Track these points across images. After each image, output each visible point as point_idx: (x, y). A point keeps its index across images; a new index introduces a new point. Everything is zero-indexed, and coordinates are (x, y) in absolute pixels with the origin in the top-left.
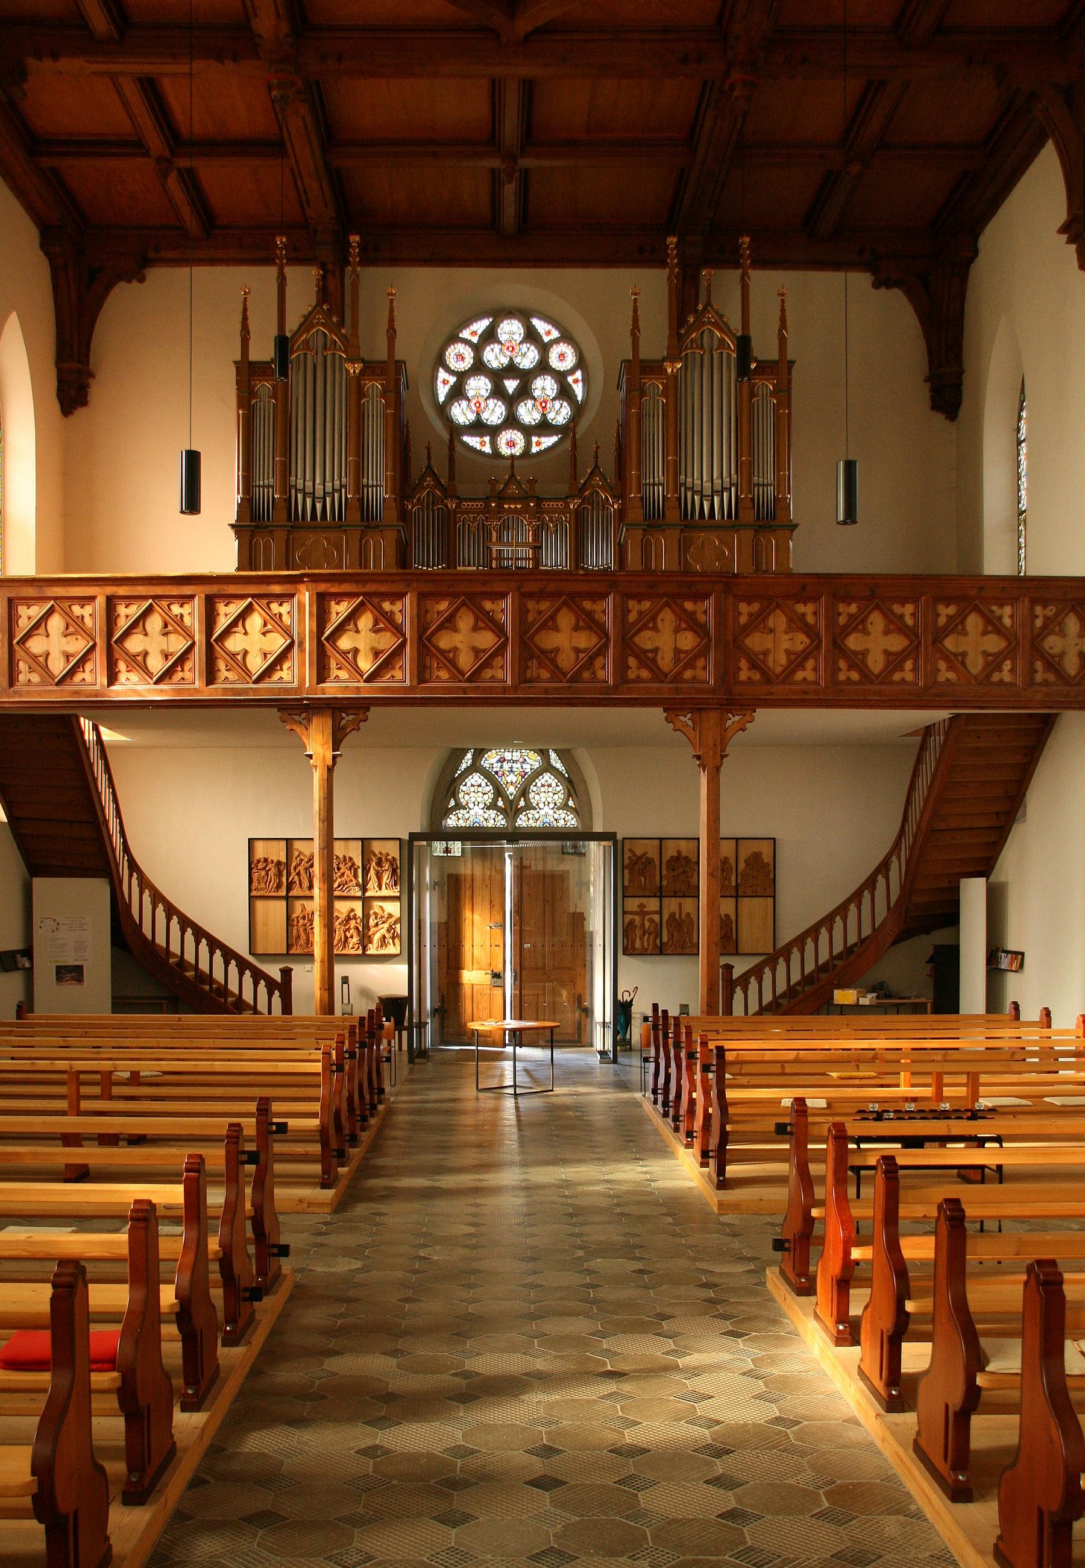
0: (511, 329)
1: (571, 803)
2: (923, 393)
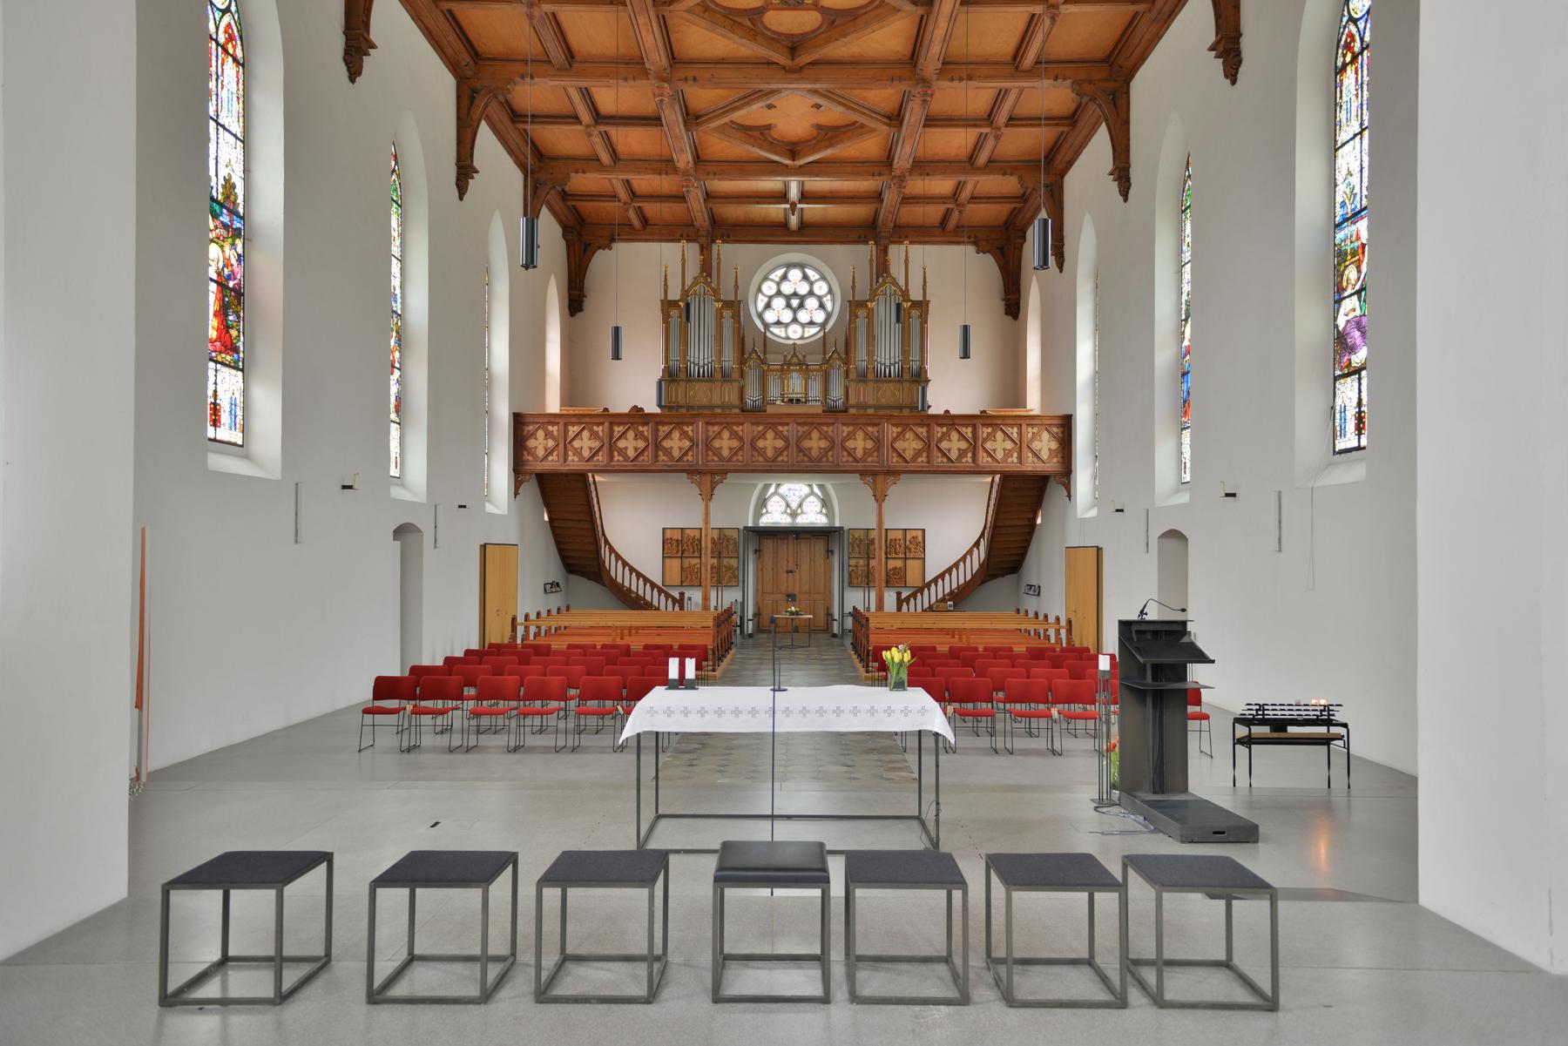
0: (795, 274)
2: (1001, 306)
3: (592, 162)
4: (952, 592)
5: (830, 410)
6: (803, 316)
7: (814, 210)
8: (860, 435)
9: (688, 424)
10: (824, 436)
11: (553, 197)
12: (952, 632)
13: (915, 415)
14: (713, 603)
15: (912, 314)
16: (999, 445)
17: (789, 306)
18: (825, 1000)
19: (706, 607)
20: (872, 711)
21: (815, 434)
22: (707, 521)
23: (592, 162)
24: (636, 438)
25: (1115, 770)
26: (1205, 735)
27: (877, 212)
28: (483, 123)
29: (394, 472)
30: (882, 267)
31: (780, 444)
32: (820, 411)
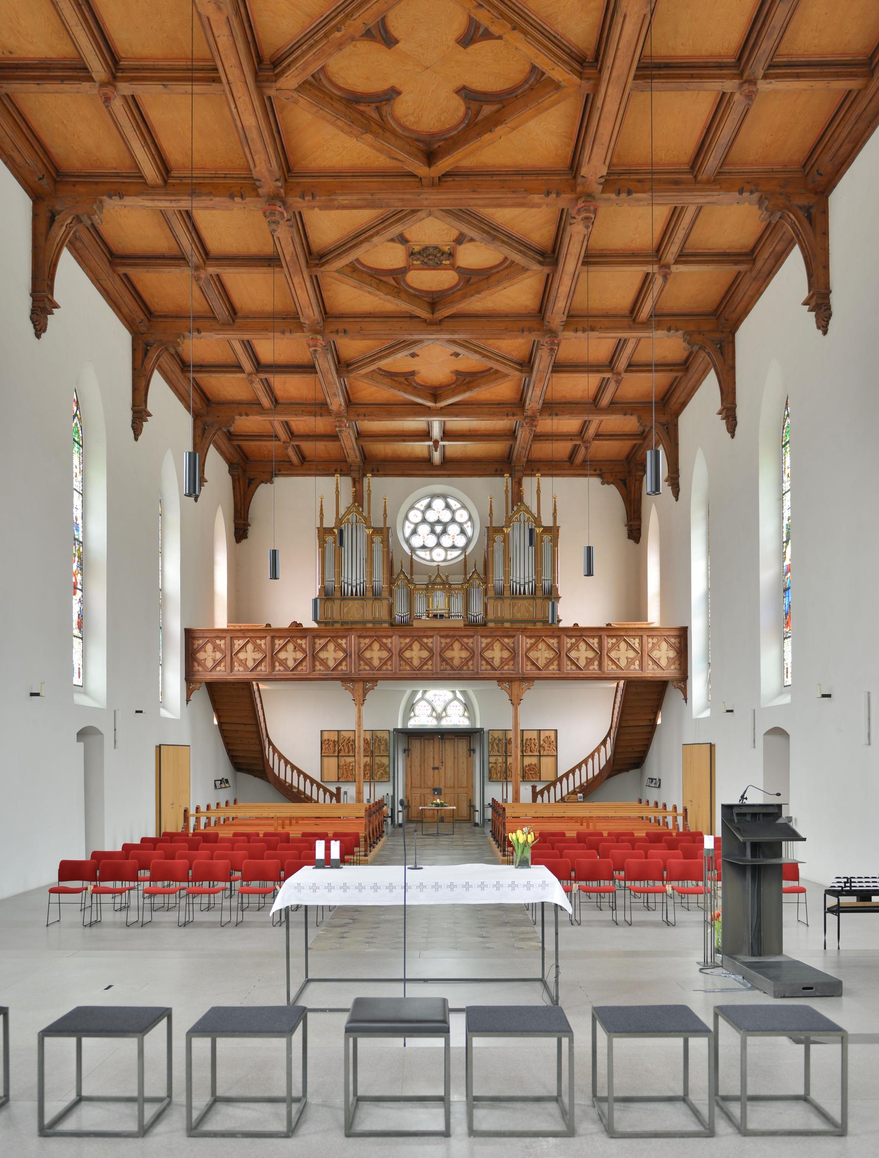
0: (438, 504)
1: (466, 714)
2: (624, 531)
3: (252, 406)
4: (581, 785)
5: (472, 625)
6: (446, 541)
7: (455, 448)
8: (497, 646)
9: (342, 637)
10: (464, 647)
11: (220, 437)
12: (581, 820)
13: (549, 628)
14: (366, 796)
15: (544, 537)
16: (623, 655)
17: (433, 532)
18: (446, 1134)
19: (359, 800)
20: (498, 886)
21: (457, 646)
22: (359, 725)
23: (252, 406)
24: (295, 650)
25: (718, 937)
26: (802, 907)
27: (511, 448)
28: (212, 446)
29: (77, 681)
30: (517, 498)
31: (425, 654)
32: (461, 625)
